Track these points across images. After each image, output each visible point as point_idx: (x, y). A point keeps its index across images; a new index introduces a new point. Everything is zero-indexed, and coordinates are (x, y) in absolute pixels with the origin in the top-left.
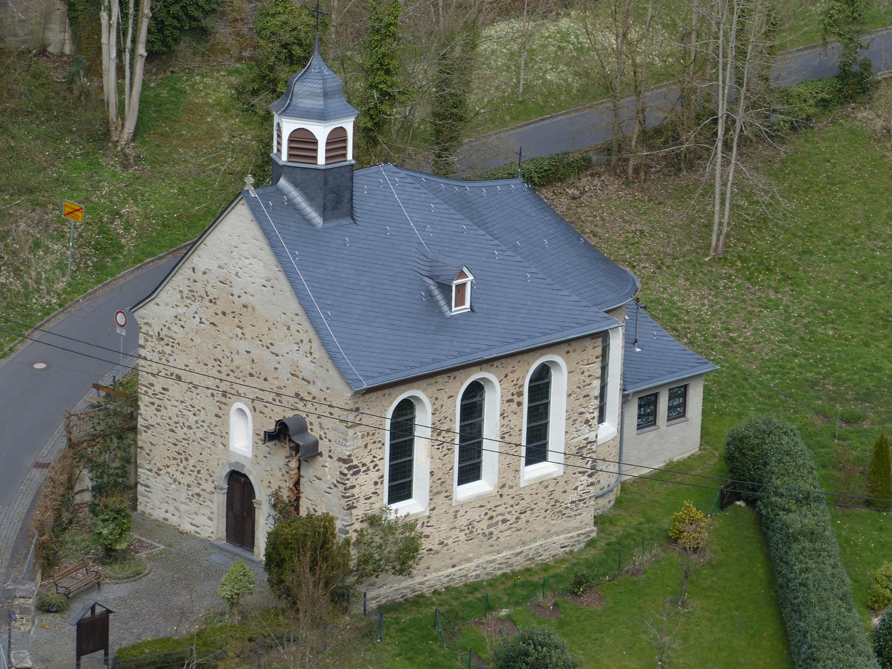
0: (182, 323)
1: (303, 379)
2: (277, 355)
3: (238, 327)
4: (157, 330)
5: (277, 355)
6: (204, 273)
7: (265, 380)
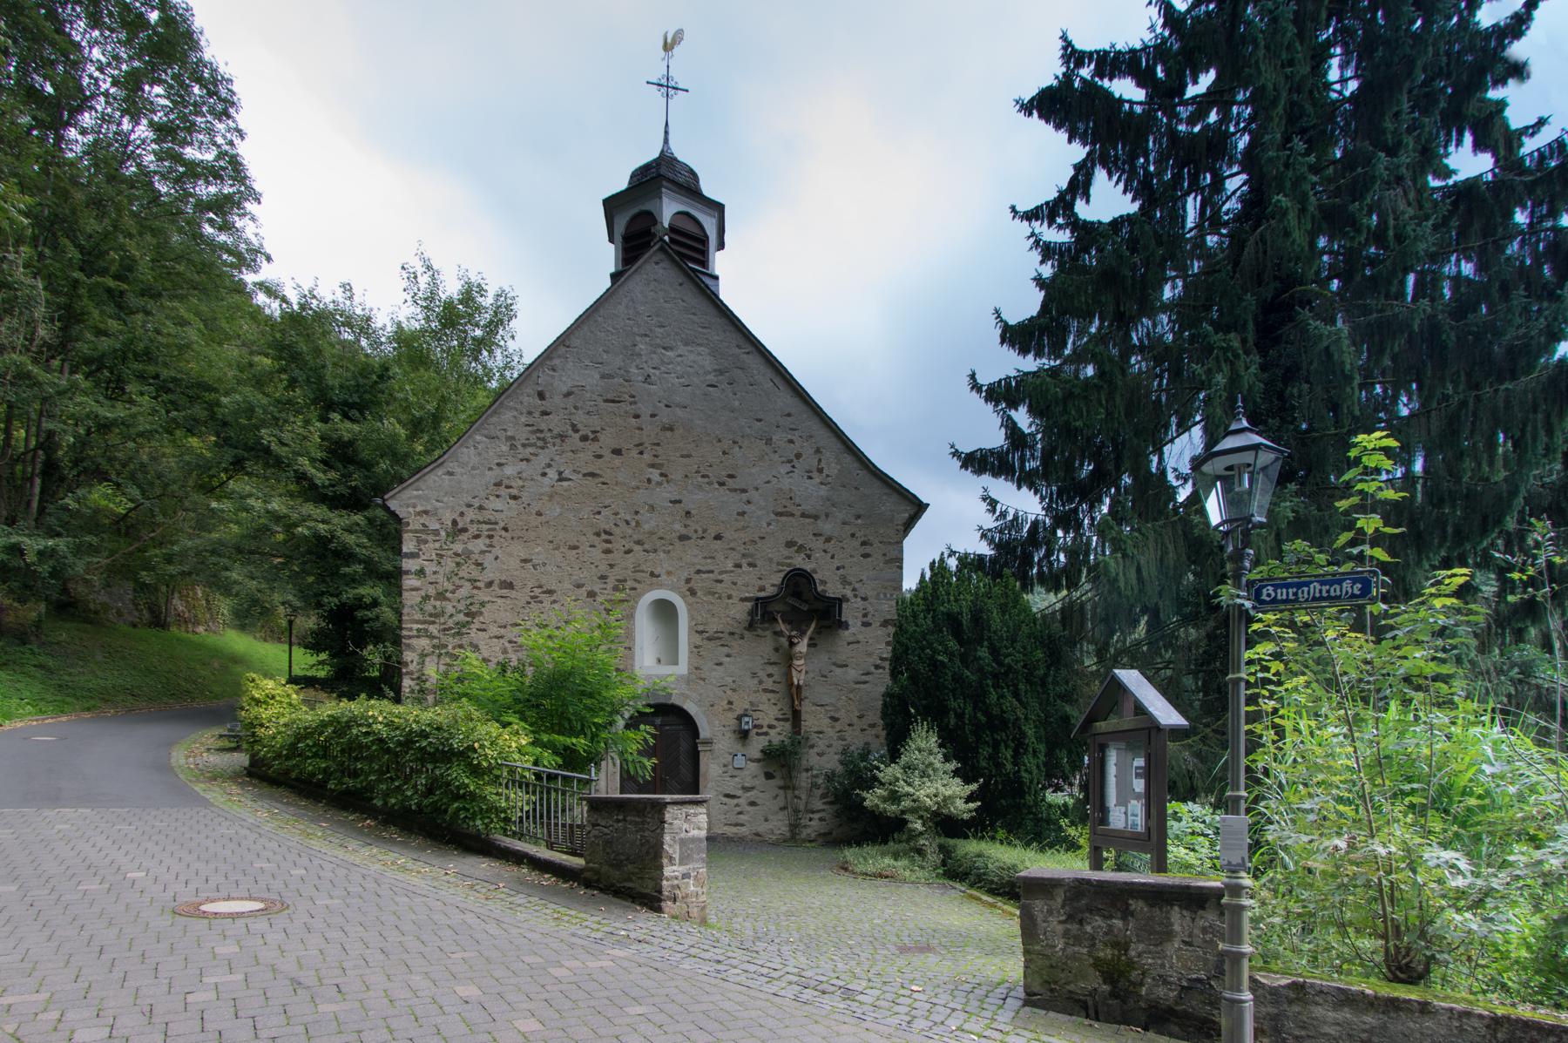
0: (514, 492)
1: (803, 515)
2: (744, 491)
3: (653, 466)
4: (448, 518)
5: (744, 491)
6: (568, 394)
7: (718, 537)
